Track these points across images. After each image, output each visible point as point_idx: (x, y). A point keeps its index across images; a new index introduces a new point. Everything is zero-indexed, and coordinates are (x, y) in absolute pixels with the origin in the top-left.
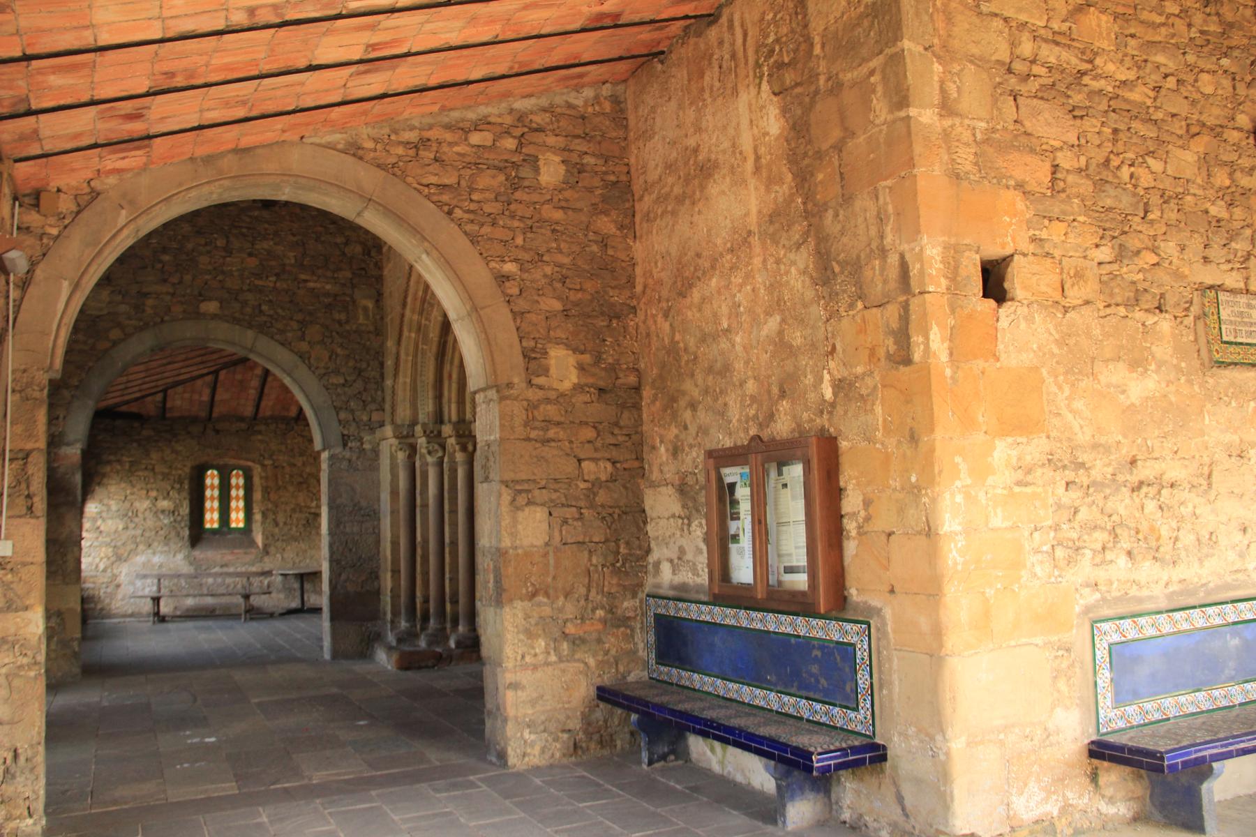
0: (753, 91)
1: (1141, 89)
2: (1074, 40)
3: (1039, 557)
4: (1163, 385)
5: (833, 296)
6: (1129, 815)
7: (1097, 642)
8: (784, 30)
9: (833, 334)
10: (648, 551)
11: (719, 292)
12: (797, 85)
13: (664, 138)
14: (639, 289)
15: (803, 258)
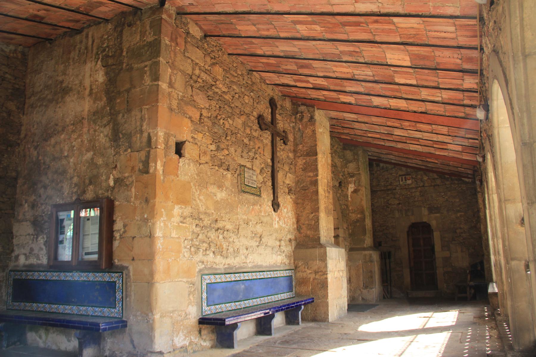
0: (94, 63)
1: (228, 95)
2: (211, 73)
3: (186, 249)
4: (227, 196)
5: (118, 146)
6: (210, 346)
7: (203, 282)
8: (111, 43)
9: (116, 160)
10: (13, 251)
11: (65, 141)
12: (114, 65)
13: (46, 74)
14: (22, 136)
15: (107, 130)
